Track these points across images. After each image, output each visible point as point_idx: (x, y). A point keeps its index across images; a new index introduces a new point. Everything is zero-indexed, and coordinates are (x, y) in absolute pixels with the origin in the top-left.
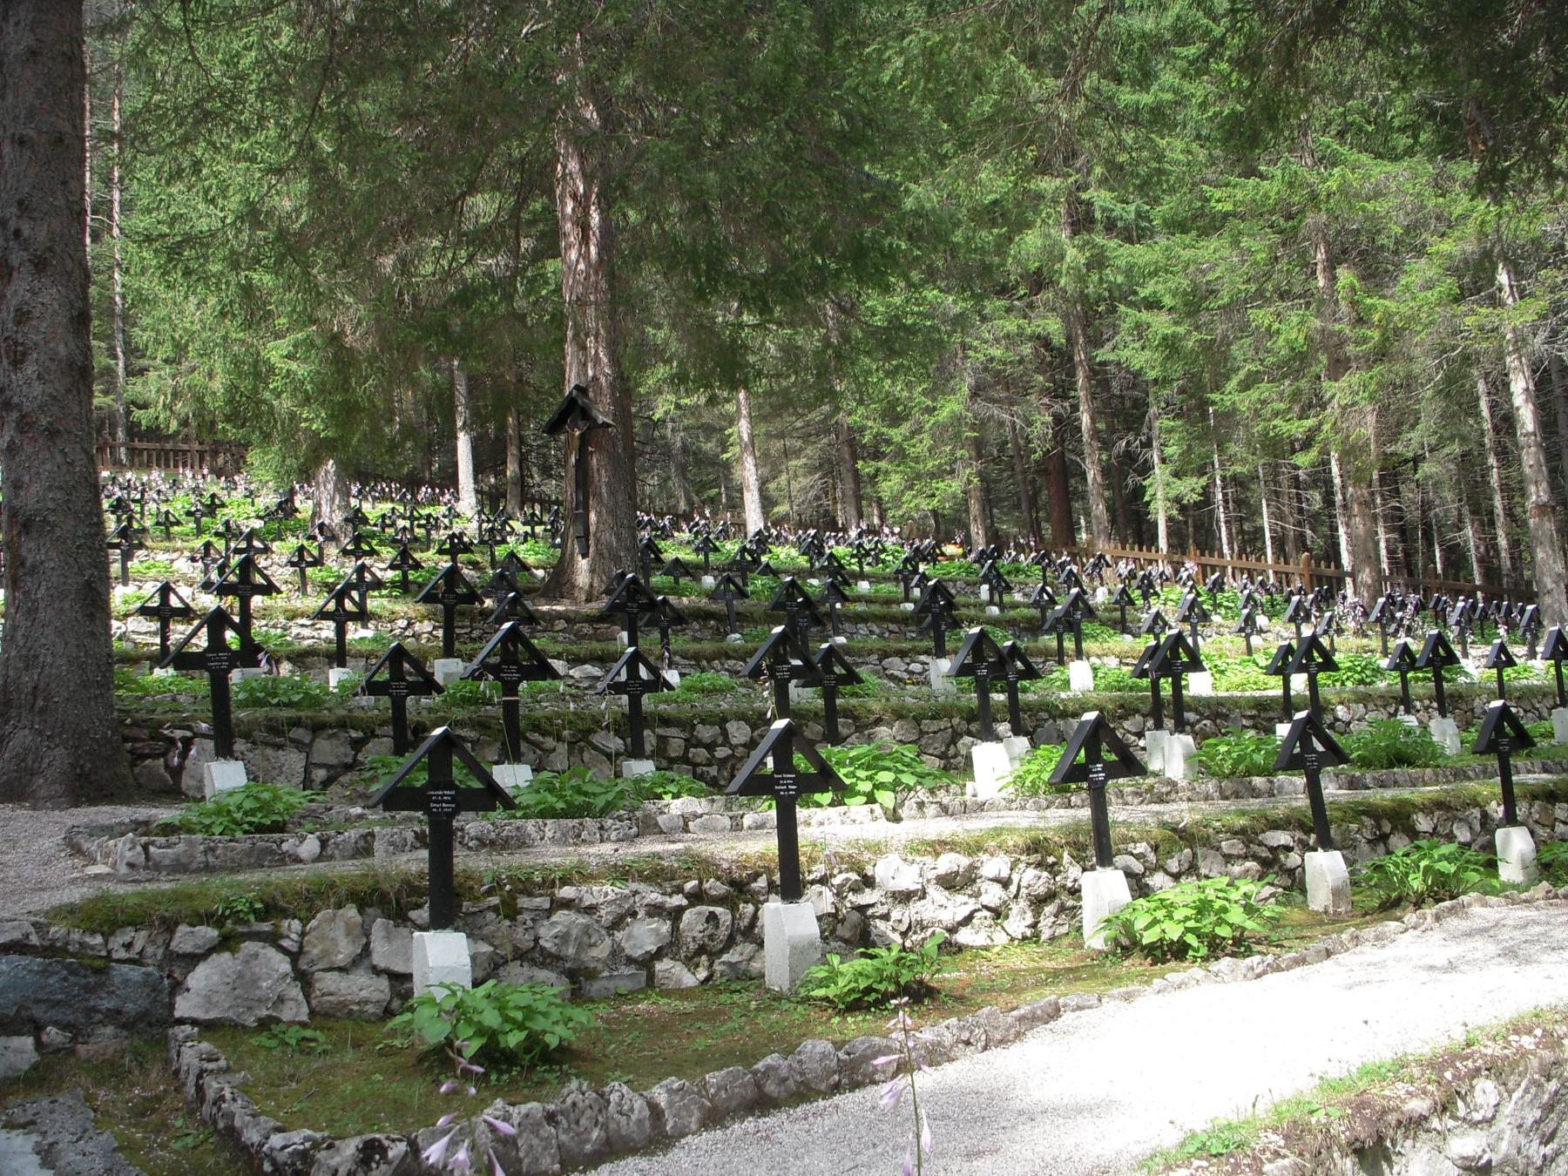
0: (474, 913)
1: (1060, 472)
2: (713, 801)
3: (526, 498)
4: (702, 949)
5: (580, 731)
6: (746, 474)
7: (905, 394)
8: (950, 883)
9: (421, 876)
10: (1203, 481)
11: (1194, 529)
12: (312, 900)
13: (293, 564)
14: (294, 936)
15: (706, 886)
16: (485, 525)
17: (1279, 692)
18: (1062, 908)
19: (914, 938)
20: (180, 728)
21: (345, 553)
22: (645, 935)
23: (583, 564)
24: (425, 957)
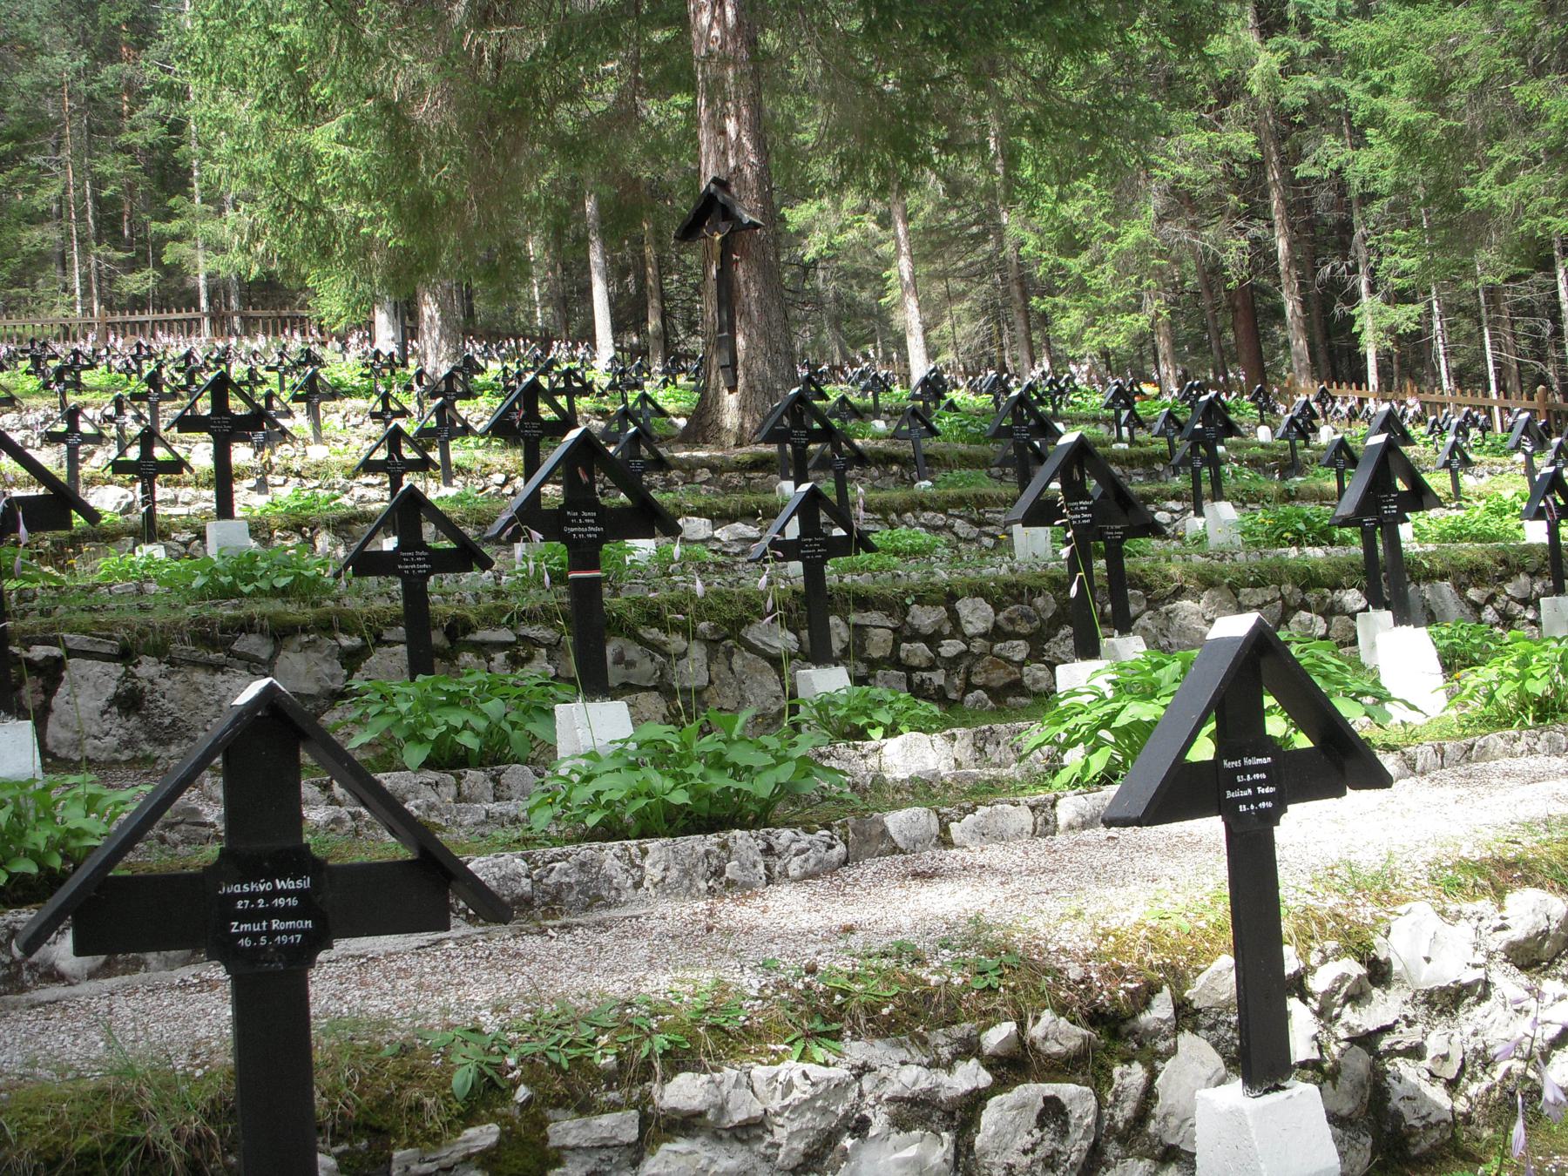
1: (1255, 310)
2: (953, 737)
5: (726, 622)
6: (909, 317)
7: (1084, 219)
10: (1420, 308)
15: (1036, 1031)
19: (1474, 1089)
20: (45, 642)
23: (730, 401)
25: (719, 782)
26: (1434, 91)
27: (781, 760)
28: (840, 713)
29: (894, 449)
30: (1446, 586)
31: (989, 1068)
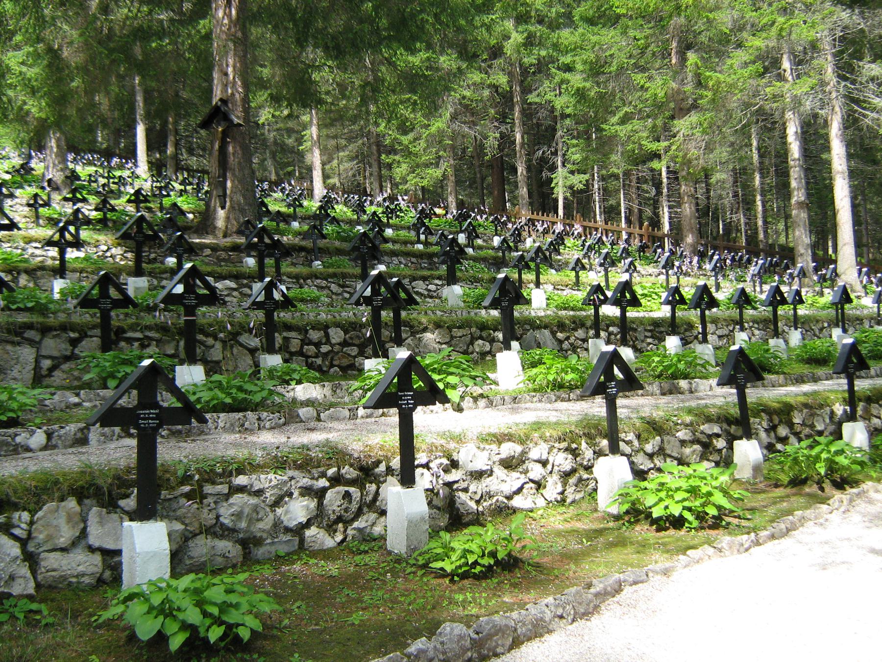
0: (170, 499)
1: (502, 168)
2: (324, 386)
3: (178, 168)
4: (339, 519)
6: (314, 160)
8: (509, 464)
9: (128, 470)
10: (587, 177)
11: (580, 203)
12: (39, 495)
13: (29, 205)
14: (24, 526)
15: (343, 471)
16: (155, 185)
17: (669, 315)
18: (580, 480)
19: (485, 504)
21: (66, 199)
22: (298, 510)
23: (221, 213)
24: (133, 544)
25: (241, 395)
26: (595, 70)
27: (263, 389)
28: (279, 374)
29: (303, 243)
30: (547, 332)
31: (329, 481)
